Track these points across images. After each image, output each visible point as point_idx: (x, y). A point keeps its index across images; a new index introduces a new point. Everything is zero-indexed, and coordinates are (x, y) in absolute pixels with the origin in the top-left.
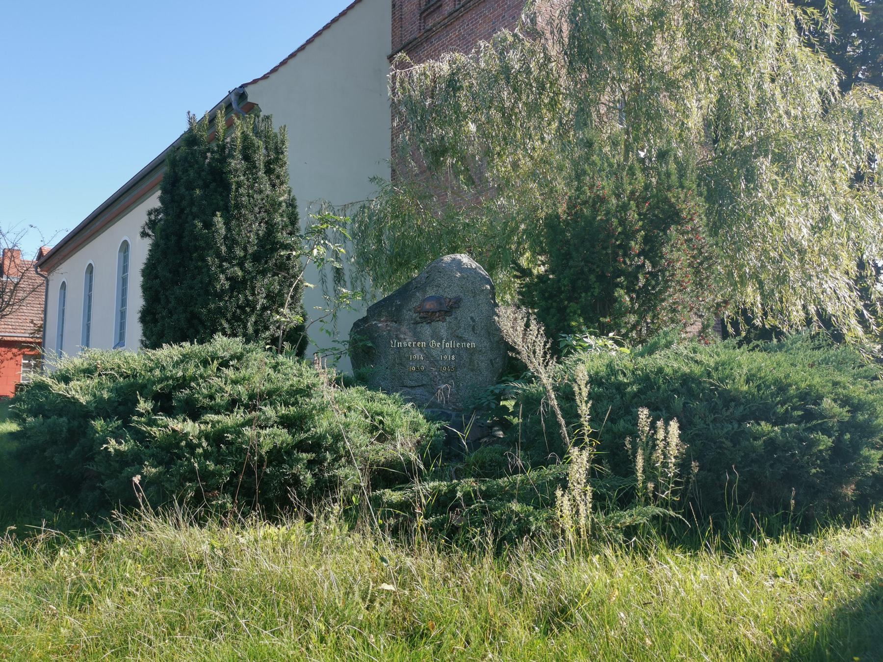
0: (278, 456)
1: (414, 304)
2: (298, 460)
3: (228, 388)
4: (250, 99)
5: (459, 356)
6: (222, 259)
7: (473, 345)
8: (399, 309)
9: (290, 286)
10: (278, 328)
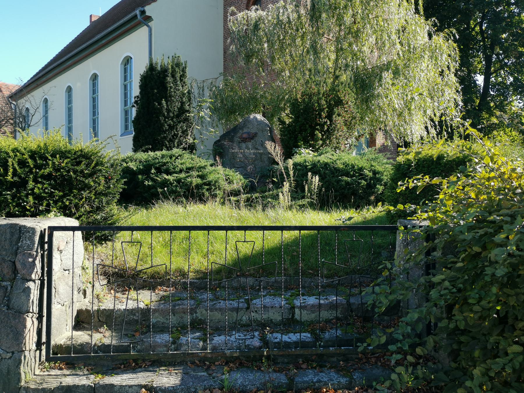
0: (198, 186)
1: (239, 135)
2: (204, 188)
3: (180, 166)
4: (148, 14)
5: (256, 156)
6: (165, 118)
7: (262, 151)
8: (233, 137)
9: (190, 127)
10: (186, 144)
